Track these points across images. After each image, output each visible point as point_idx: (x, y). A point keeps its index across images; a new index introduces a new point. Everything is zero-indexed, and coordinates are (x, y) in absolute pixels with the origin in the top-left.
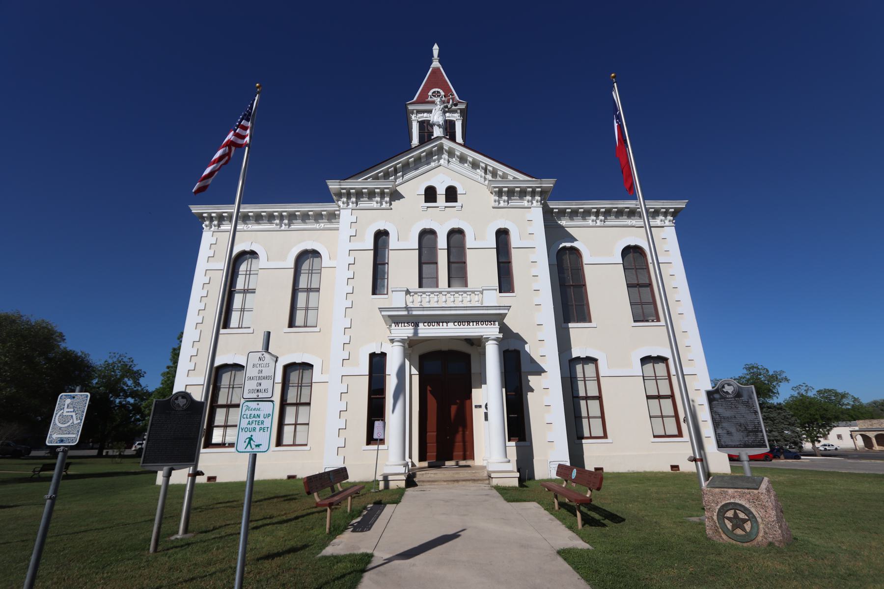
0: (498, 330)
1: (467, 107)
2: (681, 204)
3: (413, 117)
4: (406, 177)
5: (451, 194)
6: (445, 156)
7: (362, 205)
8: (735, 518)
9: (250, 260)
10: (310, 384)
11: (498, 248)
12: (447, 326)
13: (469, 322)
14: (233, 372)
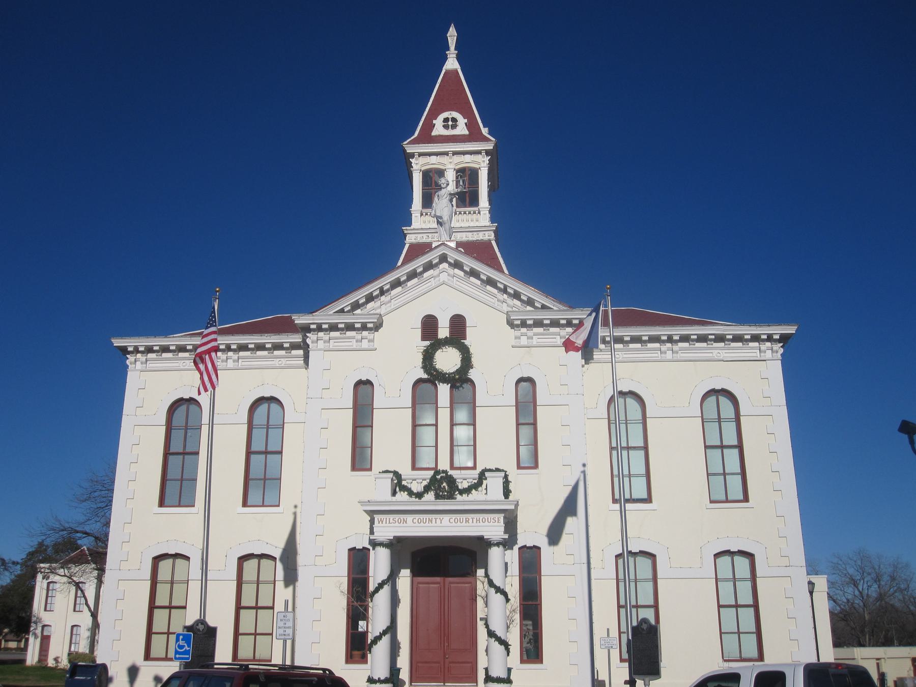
0: (503, 529)
1: (496, 146)
2: (791, 330)
12: (441, 523)
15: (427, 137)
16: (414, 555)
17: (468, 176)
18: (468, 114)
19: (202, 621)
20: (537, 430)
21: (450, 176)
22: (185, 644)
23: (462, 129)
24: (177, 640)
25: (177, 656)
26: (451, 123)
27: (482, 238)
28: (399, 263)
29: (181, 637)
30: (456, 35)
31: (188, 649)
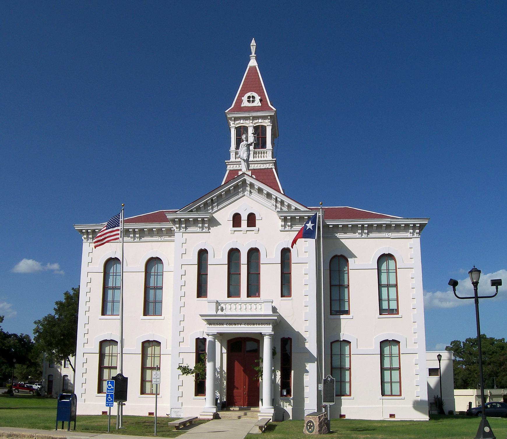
3: (232, 123)
4: (220, 207)
5: (252, 220)
6: (248, 188)
7: (190, 229)
8: (310, 428)
9: (115, 266)
10: (159, 355)
11: (281, 263)
13: (254, 324)
14: (111, 346)
15: (239, 108)
16: (229, 342)
17: (260, 131)
18: (261, 94)
19: (121, 375)
20: (145, 283)
21: (251, 131)
22: (112, 386)
23: (257, 103)
24: (108, 384)
25: (108, 391)
26: (251, 99)
27: (268, 167)
28: (223, 183)
29: (109, 382)
30: (256, 45)
31: (113, 388)
